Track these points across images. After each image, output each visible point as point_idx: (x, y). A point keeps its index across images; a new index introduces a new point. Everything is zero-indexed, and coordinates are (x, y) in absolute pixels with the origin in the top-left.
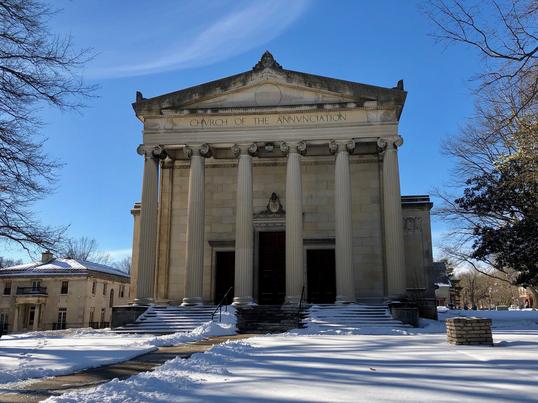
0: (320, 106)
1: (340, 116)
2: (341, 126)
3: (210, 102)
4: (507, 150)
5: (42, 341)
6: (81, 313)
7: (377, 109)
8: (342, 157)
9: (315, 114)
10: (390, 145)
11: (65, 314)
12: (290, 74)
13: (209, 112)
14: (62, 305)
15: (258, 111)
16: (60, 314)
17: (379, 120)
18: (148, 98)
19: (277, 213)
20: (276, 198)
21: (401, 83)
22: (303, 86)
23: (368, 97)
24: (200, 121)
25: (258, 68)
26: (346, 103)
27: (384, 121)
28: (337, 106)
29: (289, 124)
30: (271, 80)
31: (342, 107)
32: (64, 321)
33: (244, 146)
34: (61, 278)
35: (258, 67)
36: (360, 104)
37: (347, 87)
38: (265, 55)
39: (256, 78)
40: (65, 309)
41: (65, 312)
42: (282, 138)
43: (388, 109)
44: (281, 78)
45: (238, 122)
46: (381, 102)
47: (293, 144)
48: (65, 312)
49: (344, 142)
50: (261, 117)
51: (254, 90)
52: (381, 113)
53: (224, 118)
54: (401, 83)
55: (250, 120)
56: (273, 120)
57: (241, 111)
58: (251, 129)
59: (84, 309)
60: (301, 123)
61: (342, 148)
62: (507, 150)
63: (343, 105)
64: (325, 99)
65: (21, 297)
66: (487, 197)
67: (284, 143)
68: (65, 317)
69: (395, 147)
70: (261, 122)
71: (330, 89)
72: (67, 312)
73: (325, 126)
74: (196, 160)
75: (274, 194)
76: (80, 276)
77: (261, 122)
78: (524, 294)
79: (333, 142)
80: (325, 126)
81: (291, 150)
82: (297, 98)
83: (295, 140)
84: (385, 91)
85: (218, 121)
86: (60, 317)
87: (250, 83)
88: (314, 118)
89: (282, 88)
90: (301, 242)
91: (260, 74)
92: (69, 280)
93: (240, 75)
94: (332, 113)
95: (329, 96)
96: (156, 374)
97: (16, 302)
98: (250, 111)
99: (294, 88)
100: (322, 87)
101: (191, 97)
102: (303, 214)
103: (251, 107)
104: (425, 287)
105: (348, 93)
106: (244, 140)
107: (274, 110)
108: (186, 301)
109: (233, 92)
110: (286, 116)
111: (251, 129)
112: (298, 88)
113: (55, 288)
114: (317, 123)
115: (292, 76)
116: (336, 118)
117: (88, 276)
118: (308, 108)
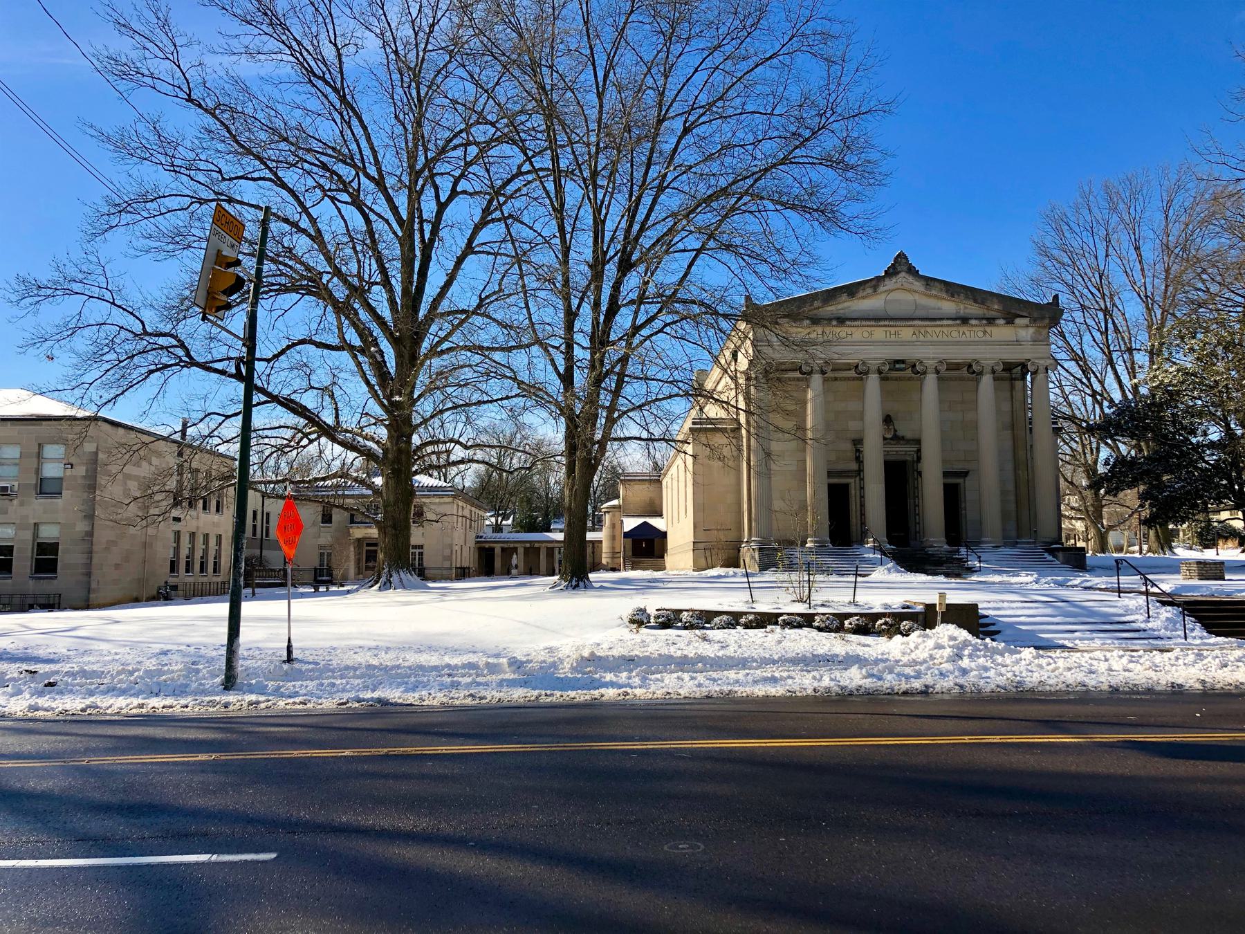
0: (965, 320)
1: (985, 332)
2: (986, 343)
6: (447, 552)
7: (1027, 326)
8: (987, 380)
9: (955, 328)
11: (421, 554)
12: (929, 281)
13: (834, 323)
19: (891, 439)
21: (1056, 297)
22: (944, 295)
23: (1018, 312)
24: (820, 332)
25: (891, 272)
26: (994, 319)
27: (1035, 341)
28: (984, 322)
30: (906, 286)
33: (873, 365)
35: (891, 270)
36: (1010, 320)
37: (995, 300)
39: (890, 284)
40: (421, 547)
42: (918, 356)
43: (1039, 327)
44: (918, 285)
45: (866, 334)
46: (1034, 320)
47: (931, 364)
49: (991, 363)
50: (893, 330)
51: (883, 296)
52: (1031, 330)
53: (849, 330)
55: (879, 333)
56: (906, 333)
57: (872, 323)
59: (451, 546)
60: (940, 338)
61: (988, 369)
63: (991, 321)
64: (967, 311)
65: (358, 528)
68: (421, 559)
71: (976, 301)
72: (426, 551)
74: (817, 379)
75: (888, 416)
76: (442, 496)
79: (978, 362)
81: (929, 370)
83: (933, 359)
84: (1038, 306)
85: (842, 331)
86: (321, 560)
87: (881, 289)
89: (917, 297)
90: (941, 475)
91: (894, 280)
95: (972, 309)
96: (973, 578)
97: (349, 535)
98: (882, 323)
99: (931, 296)
100: (967, 297)
101: (812, 305)
103: (885, 319)
110: (922, 330)
111: (883, 343)
112: (936, 297)
114: (958, 339)
116: (981, 334)
117: (454, 497)
118: (950, 322)
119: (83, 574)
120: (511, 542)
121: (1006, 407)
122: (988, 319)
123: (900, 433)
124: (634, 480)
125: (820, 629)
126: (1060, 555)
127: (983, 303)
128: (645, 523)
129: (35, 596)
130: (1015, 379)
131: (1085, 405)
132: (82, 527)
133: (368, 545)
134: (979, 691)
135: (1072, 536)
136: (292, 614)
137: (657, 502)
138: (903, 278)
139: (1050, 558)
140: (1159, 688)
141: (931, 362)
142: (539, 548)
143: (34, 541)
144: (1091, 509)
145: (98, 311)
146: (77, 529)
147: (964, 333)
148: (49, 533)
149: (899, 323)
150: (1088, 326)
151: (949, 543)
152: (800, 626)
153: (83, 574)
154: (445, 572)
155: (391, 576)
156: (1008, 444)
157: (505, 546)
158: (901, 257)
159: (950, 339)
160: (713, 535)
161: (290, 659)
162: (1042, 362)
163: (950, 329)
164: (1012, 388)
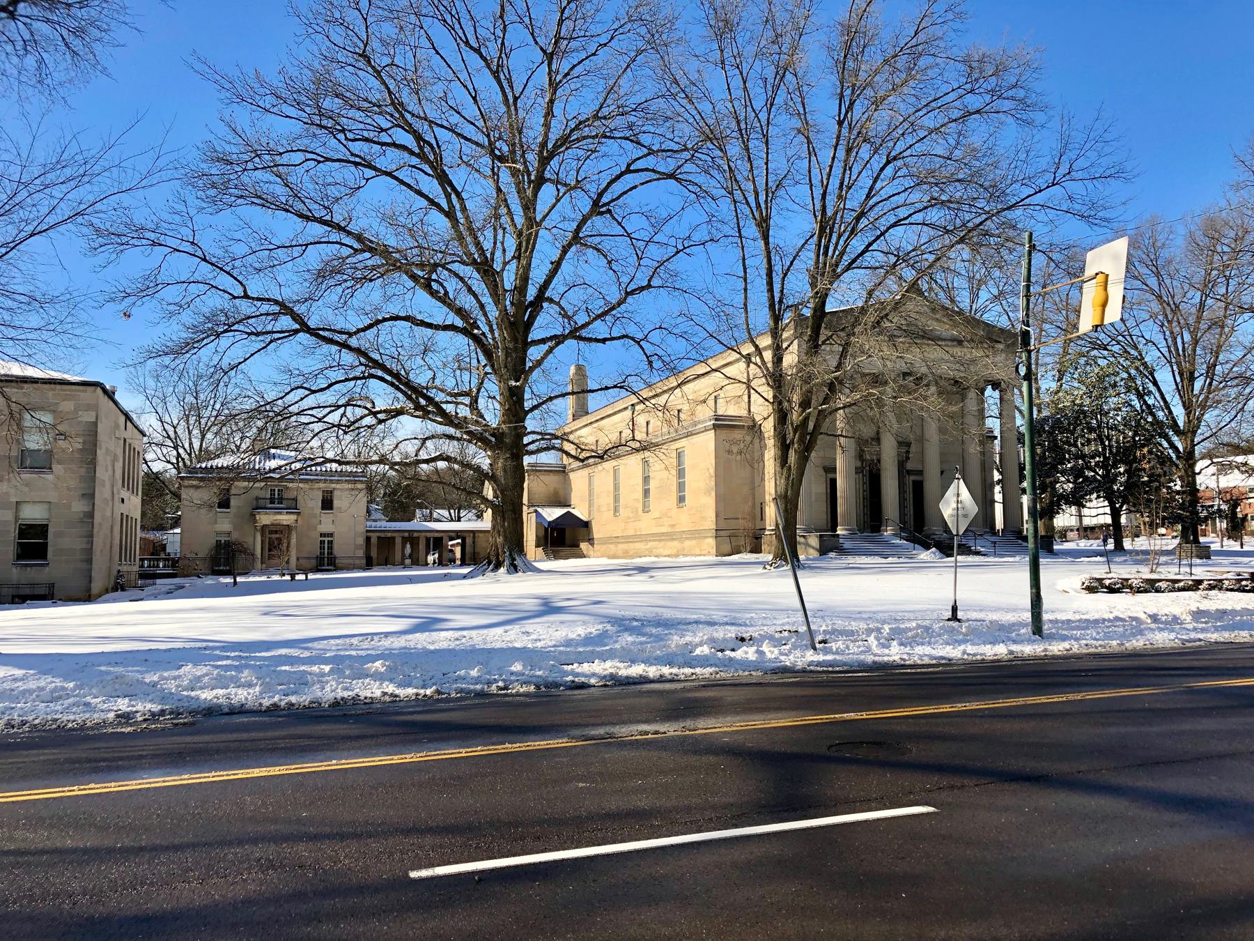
4: (1101, 511)
5: (689, 723)
11: (330, 543)
14: (326, 527)
16: (322, 542)
18: (543, 187)
32: (330, 553)
34: (322, 485)
40: (331, 535)
62: (1101, 511)
65: (267, 513)
78: (880, 403)
86: (322, 548)
97: (255, 521)
102: (942, 473)
104: (569, 366)
113: (311, 502)
119: (82, 561)
120: (388, 531)
124: (540, 471)
125: (1227, 590)
128: (568, 513)
129: (18, 586)
132: (79, 507)
133: (271, 532)
134: (795, 666)
136: (953, 575)
137: (561, 493)
140: (798, 667)
142: (418, 538)
143: (16, 521)
145: (183, 266)
146: (74, 509)
148: (33, 514)
152: (1146, 591)
153: (82, 561)
155: (514, 559)
157: (382, 535)
160: (733, 524)
161: (954, 617)
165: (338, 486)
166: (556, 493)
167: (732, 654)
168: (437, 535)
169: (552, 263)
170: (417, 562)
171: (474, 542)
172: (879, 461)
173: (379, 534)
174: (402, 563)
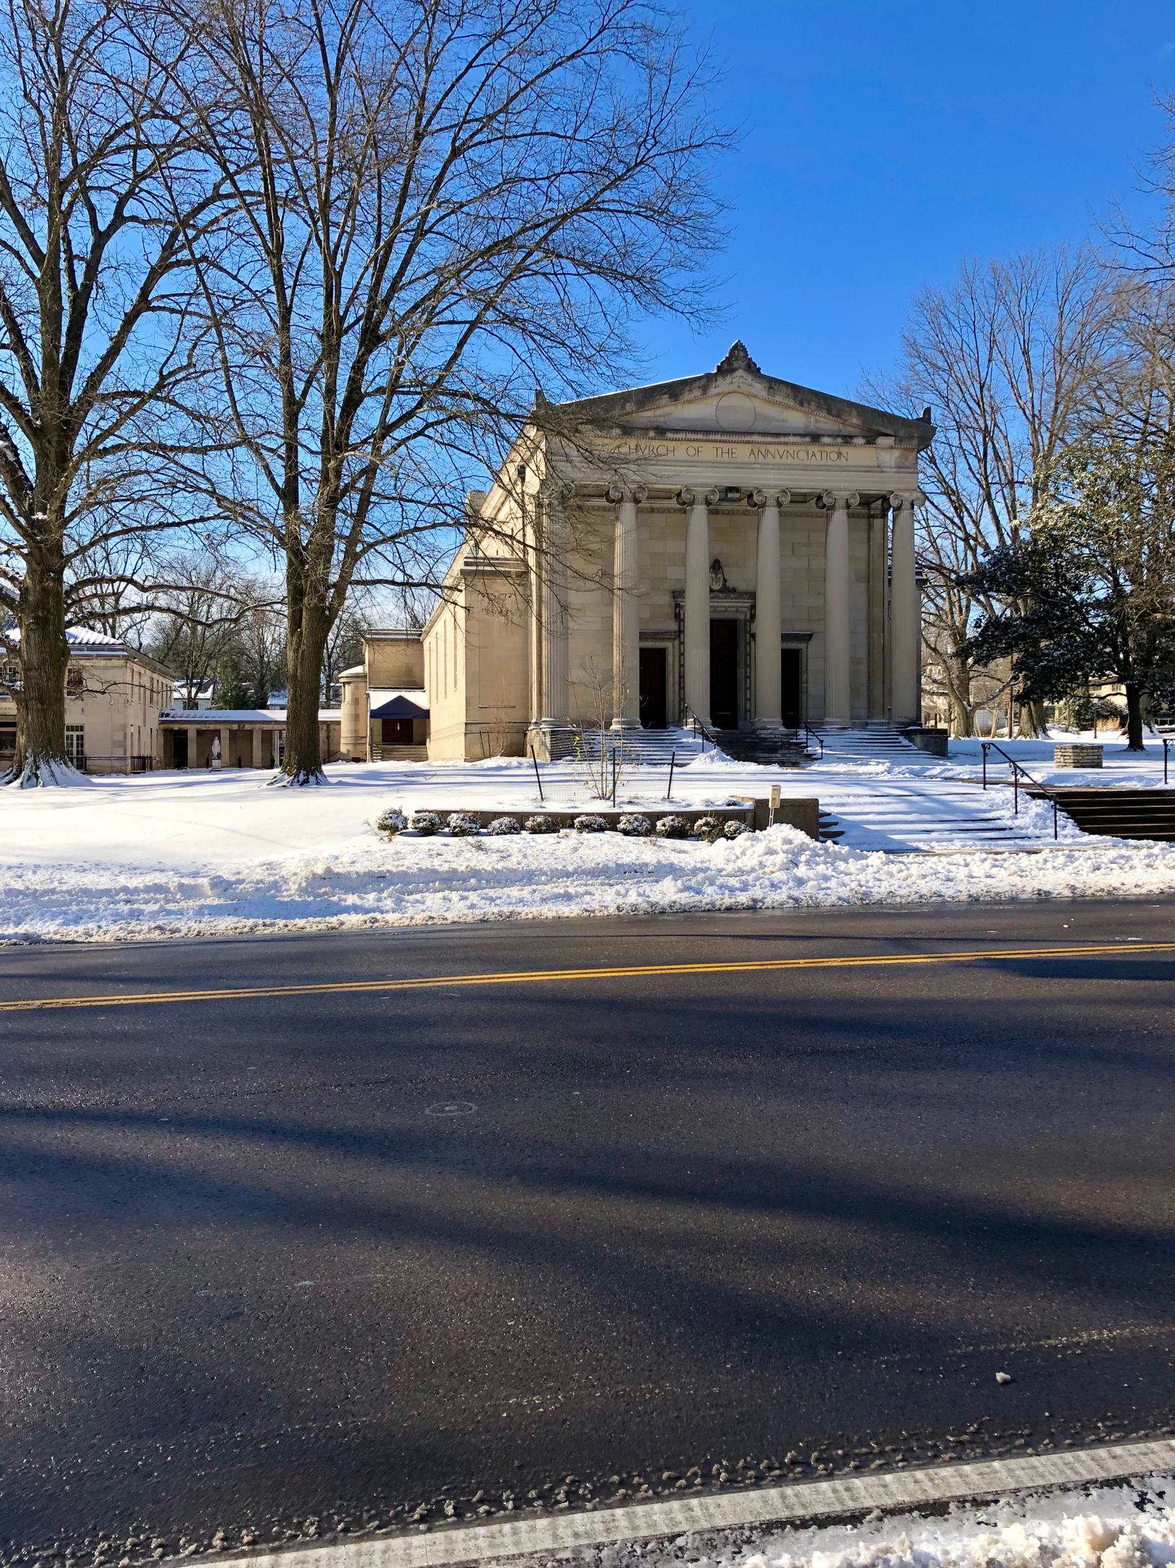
0: (815, 438)
1: (839, 454)
3: (648, 415)
7: (892, 448)
8: (839, 518)
9: (803, 448)
10: (906, 504)
11: (80, 738)
12: (773, 384)
13: (652, 434)
15: (725, 438)
17: (893, 465)
19: (720, 591)
20: (720, 568)
21: (928, 411)
22: (791, 403)
25: (725, 369)
26: (852, 437)
28: (840, 440)
29: (766, 461)
30: (745, 388)
31: (847, 442)
35: (726, 366)
36: (871, 439)
37: (854, 412)
38: (736, 346)
39: (723, 384)
40: (81, 728)
41: (80, 733)
43: (906, 449)
44: (759, 388)
45: (692, 452)
46: (899, 440)
47: (771, 494)
48: (80, 733)
50: (726, 447)
51: (715, 401)
52: (896, 453)
53: (671, 445)
54: (928, 411)
55: (708, 451)
56: (742, 452)
57: (700, 436)
58: (713, 464)
60: (784, 460)
61: (842, 503)
63: (847, 439)
64: (819, 425)
66: (1042, 645)
67: (759, 491)
68: (81, 745)
69: (912, 505)
70: (725, 455)
71: (829, 413)
72: (87, 733)
73: (819, 468)
76: (110, 658)
77: (725, 455)
80: (819, 468)
82: (778, 420)
83: (775, 487)
87: (713, 391)
88: (805, 454)
91: (729, 379)
92: (83, 666)
93: (699, 378)
94: (829, 449)
95: (824, 422)
98: (712, 437)
99: (774, 403)
100: (819, 407)
101: (623, 408)
103: (716, 432)
105: (855, 421)
106: (700, 481)
107: (748, 438)
108: (618, 722)
109: (690, 402)
111: (713, 464)
112: (779, 404)
114: (806, 462)
115: (776, 387)
116: (834, 456)
118: (797, 439)
120: (211, 722)
121: (862, 552)
122: (844, 437)
123: (730, 584)
124: (385, 640)
126: (918, 739)
127: (839, 416)
130: (873, 517)
131: (956, 552)
135: (932, 716)
138: (740, 376)
139: (906, 742)
141: (772, 491)
142: (251, 731)
144: (956, 682)
147: (814, 455)
149: (734, 438)
150: (964, 450)
151: (785, 725)
152: (601, 829)
154: (117, 764)
156: (862, 600)
157: (202, 727)
158: (739, 348)
159: (796, 461)
160: (492, 715)
162: (907, 495)
163: (797, 448)
164: (870, 527)
165: (88, 663)
166: (409, 671)
167: (143, 907)
168: (266, 727)
169: (111, 339)
170: (241, 762)
171: (328, 738)
172: (753, 617)
173: (199, 726)
174: (208, 764)
